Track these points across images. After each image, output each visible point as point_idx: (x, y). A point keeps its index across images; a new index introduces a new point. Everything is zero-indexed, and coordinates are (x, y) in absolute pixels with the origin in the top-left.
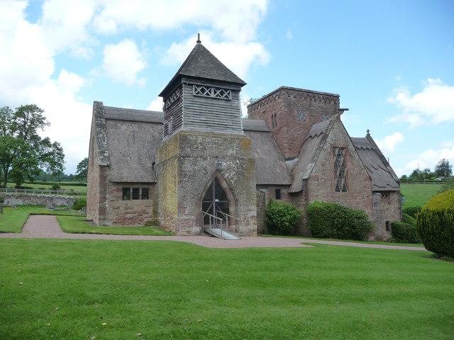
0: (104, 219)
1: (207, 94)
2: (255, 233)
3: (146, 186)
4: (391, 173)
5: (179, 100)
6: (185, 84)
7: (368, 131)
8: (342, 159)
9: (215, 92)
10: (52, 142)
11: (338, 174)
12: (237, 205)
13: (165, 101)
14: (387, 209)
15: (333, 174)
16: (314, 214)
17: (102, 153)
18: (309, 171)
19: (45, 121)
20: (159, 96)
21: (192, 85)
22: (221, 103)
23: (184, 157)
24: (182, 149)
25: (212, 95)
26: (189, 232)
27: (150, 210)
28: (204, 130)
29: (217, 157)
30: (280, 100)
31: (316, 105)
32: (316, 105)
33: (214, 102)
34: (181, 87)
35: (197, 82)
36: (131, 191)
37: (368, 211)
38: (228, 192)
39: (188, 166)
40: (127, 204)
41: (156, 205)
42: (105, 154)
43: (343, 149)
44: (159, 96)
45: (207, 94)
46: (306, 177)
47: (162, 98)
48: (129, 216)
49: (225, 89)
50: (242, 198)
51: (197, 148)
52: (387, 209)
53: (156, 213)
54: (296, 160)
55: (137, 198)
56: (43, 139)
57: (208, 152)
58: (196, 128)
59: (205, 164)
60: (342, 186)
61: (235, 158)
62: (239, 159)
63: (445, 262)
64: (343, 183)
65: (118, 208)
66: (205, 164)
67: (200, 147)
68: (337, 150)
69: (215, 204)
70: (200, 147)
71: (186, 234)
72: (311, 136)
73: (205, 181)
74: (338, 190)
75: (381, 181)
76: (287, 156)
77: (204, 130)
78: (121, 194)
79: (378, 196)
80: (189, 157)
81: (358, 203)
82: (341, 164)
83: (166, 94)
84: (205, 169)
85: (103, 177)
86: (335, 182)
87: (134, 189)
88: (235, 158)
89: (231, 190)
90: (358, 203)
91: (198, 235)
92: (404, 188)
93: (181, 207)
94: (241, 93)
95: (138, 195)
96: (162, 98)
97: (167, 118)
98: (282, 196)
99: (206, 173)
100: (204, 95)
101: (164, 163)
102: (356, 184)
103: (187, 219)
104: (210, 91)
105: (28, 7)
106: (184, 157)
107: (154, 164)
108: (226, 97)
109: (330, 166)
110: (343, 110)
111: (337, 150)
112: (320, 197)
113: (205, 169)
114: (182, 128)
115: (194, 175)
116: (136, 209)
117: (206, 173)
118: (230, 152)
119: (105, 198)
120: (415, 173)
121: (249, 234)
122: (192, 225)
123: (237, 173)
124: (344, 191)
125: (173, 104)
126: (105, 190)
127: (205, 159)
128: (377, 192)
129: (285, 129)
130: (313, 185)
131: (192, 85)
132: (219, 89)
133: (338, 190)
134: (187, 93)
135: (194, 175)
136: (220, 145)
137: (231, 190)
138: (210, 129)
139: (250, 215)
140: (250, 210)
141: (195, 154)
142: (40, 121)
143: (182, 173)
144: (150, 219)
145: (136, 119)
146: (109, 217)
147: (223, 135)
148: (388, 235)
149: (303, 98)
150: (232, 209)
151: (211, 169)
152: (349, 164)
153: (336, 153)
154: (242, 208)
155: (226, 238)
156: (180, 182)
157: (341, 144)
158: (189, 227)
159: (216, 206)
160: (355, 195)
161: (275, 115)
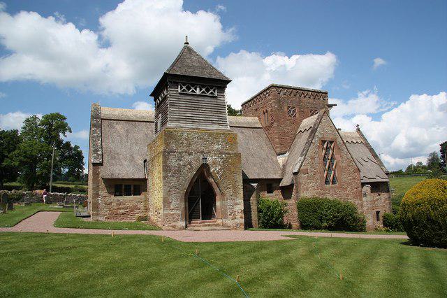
0: (97, 215)
1: (193, 91)
2: (243, 227)
3: (136, 183)
4: (380, 164)
5: (165, 98)
6: (171, 82)
8: (331, 152)
9: (181, 88)
10: (73, 146)
11: (327, 167)
13: (155, 100)
14: (377, 200)
15: (322, 167)
16: (304, 207)
17: (95, 151)
18: (299, 165)
22: (206, 99)
24: (167, 144)
25: (198, 92)
27: (141, 206)
28: (190, 126)
29: (202, 152)
30: (270, 97)
31: (306, 101)
32: (305, 100)
33: (200, 99)
36: (123, 187)
37: (357, 202)
38: (215, 186)
39: (173, 162)
41: (147, 200)
43: (331, 142)
44: (151, 95)
45: (193, 91)
46: (296, 171)
48: (121, 211)
49: (191, 84)
50: (228, 192)
51: (182, 143)
52: (377, 200)
53: (147, 209)
54: (287, 154)
56: (64, 142)
57: (193, 147)
58: (182, 124)
59: (190, 158)
60: (331, 178)
61: (221, 153)
62: (225, 154)
65: (111, 203)
66: (190, 158)
69: (200, 199)
70: (185, 142)
71: (171, 228)
72: (301, 131)
73: (189, 175)
74: (327, 182)
75: (372, 173)
76: (278, 150)
79: (367, 188)
82: (330, 157)
84: (190, 165)
85: (96, 174)
87: (134, 186)
88: (221, 153)
91: (183, 229)
92: (393, 183)
93: (166, 202)
94: (227, 90)
97: (157, 116)
99: (192, 168)
101: (152, 160)
102: (344, 177)
103: (173, 214)
106: (169, 153)
107: (145, 161)
108: (212, 93)
109: (319, 160)
110: (331, 106)
112: (309, 191)
113: (190, 165)
114: (168, 125)
116: (128, 204)
119: (98, 195)
120: (409, 168)
121: (236, 227)
123: (223, 168)
124: (334, 183)
125: (161, 102)
126: (98, 186)
128: (368, 183)
129: (275, 124)
137: (217, 184)
138: (194, 126)
141: (180, 150)
142: (64, 128)
143: (166, 168)
144: (142, 215)
145: (132, 118)
146: (102, 212)
147: (209, 130)
148: (380, 224)
151: (196, 165)
153: (325, 146)
155: (202, 233)
156: (165, 178)
157: (329, 137)
158: (174, 221)
161: (267, 112)
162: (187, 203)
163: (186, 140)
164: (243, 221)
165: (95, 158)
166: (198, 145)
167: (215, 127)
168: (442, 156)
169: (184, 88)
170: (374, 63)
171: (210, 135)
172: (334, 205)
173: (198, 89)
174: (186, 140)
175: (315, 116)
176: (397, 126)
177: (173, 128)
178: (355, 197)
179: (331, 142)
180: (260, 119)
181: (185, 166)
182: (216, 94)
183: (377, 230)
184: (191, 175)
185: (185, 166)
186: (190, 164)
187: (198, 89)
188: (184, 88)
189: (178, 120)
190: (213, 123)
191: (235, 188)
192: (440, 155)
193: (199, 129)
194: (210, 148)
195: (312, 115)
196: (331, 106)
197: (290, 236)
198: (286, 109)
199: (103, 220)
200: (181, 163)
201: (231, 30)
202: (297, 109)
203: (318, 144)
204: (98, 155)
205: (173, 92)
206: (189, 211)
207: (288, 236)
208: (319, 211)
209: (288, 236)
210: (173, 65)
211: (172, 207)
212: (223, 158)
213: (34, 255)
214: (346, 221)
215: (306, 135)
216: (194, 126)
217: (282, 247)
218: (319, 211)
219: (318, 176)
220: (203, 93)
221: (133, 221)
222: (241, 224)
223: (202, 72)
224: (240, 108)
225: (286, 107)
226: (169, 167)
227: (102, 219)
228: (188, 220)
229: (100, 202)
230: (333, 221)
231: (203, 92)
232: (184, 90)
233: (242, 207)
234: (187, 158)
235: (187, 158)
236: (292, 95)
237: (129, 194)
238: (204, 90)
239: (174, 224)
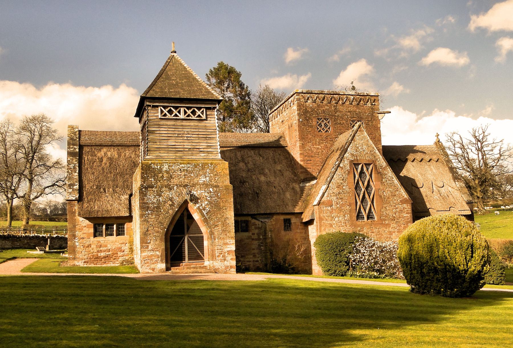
0: (74, 259)
1: (199, 116)
2: (234, 270)
9: (185, 112)
19: (56, 135)
20: (135, 116)
21: (157, 106)
22: (192, 123)
23: (146, 188)
25: (182, 116)
27: (126, 248)
33: (185, 123)
34: (145, 109)
35: (171, 103)
39: (151, 198)
43: (368, 165)
44: (135, 116)
48: (102, 254)
49: (197, 108)
51: (163, 176)
55: (112, 235)
57: (175, 181)
62: (213, 186)
63: (249, 282)
67: (165, 175)
70: (165, 175)
73: (169, 212)
78: (92, 230)
80: (152, 187)
83: (139, 113)
95: (239, 230)
98: (293, 226)
100: (172, 117)
104: (179, 112)
106: (146, 188)
108: (199, 116)
109: (348, 187)
115: (158, 208)
116: (109, 247)
117: (172, 205)
122: (157, 262)
123: (210, 203)
131: (157, 106)
132: (191, 108)
133: (359, 216)
135: (158, 208)
136: (190, 172)
139: (226, 250)
144: (127, 258)
160: (387, 222)
162: (169, 244)
164: (234, 263)
169: (189, 112)
170: (500, 48)
174: (166, 171)
181: (165, 202)
185: (165, 202)
186: (171, 199)
194: (196, 180)
201: (421, 33)
203: (348, 167)
206: (171, 253)
210: (151, 87)
212: (211, 192)
213: (332, 326)
215: (339, 152)
221: (117, 265)
222: (231, 267)
223: (162, 92)
224: (136, 125)
226: (147, 203)
228: (169, 262)
229: (77, 244)
233: (233, 248)
239: (153, 266)
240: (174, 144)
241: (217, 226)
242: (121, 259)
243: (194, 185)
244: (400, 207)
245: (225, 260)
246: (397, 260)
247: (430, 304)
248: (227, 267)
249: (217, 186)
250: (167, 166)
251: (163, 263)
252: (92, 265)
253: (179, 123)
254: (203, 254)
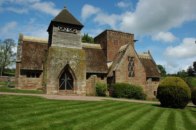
0: (17, 86)
1: (65, 30)
7: (149, 51)
9: (60, 28)
12: (76, 81)
22: (71, 34)
25: (68, 31)
26: (52, 93)
28: (62, 46)
29: (67, 59)
32: (123, 38)
37: (144, 86)
40: (28, 80)
42: (20, 57)
43: (133, 58)
46: (114, 70)
47: (48, 32)
50: (79, 78)
51: (58, 54)
54: (112, 62)
57: (63, 56)
61: (76, 60)
62: (78, 60)
64: (132, 73)
65: (24, 81)
67: (59, 54)
68: (130, 58)
70: (59, 54)
71: (50, 93)
74: (129, 76)
77: (62, 46)
81: (139, 83)
86: (129, 73)
88: (76, 60)
89: (74, 74)
90: (139, 83)
96: (48, 32)
103: (51, 87)
105: (114, 14)
106: (51, 58)
108: (74, 31)
111: (130, 58)
116: (33, 82)
118: (74, 57)
120: (178, 73)
124: (133, 77)
127: (61, 59)
130: (117, 74)
134: (55, 29)
140: (83, 84)
141: (56, 57)
147: (71, 48)
149: (117, 35)
150: (74, 83)
151: (64, 65)
152: (135, 65)
153: (130, 59)
154: (79, 83)
155: (66, 96)
157: (132, 55)
158: (52, 90)
159: (67, 82)
161: (104, 42)
163: (60, 52)
165: (18, 59)
166: (65, 55)
167: (75, 47)
168: (194, 68)
171: (72, 51)
172: (131, 87)
173: (68, 29)
175: (126, 45)
176: (176, 58)
177: (54, 47)
178: (143, 84)
179: (133, 58)
180: (101, 45)
182: (76, 32)
183: (153, 100)
184: (61, 69)
187: (68, 29)
188: (61, 28)
189: (57, 43)
190: (74, 45)
191: (82, 76)
192: (193, 67)
193: (67, 48)
195: (126, 44)
196: (135, 41)
197: (104, 100)
198: (113, 41)
199: (20, 89)
200: (57, 63)
202: (119, 41)
204: (19, 58)
205: (55, 29)
207: (102, 100)
208: (124, 89)
209: (102, 100)
211: (51, 84)
214: (136, 94)
216: (65, 46)
217: (107, 104)
218: (124, 89)
219: (125, 73)
220: (70, 31)
225: (113, 40)
227: (20, 88)
230: (130, 94)
231: (70, 31)
232: (61, 29)
234: (60, 61)
235: (60, 61)
236: (117, 35)
237: (33, 77)
238: (70, 30)
240: (63, 41)
241: (79, 76)
242: (37, 87)
243: (71, 59)
244: (142, 73)
245: (82, 90)
246: (42, 70)
247: (9, 73)
248: (82, 93)
249: (80, 60)
250: (60, 50)
251: (56, 90)
252: (25, 89)
253: (66, 33)
254: (73, 87)
